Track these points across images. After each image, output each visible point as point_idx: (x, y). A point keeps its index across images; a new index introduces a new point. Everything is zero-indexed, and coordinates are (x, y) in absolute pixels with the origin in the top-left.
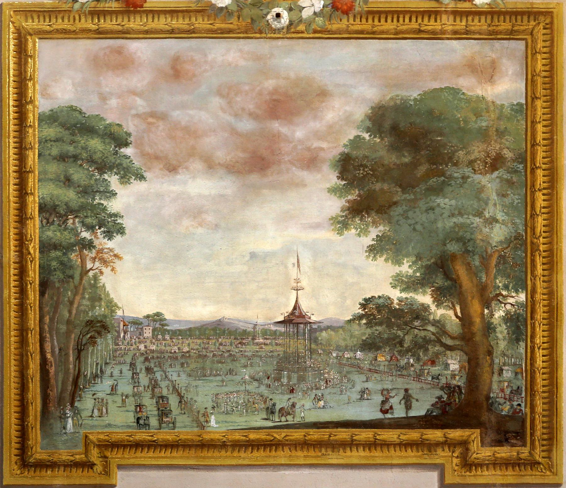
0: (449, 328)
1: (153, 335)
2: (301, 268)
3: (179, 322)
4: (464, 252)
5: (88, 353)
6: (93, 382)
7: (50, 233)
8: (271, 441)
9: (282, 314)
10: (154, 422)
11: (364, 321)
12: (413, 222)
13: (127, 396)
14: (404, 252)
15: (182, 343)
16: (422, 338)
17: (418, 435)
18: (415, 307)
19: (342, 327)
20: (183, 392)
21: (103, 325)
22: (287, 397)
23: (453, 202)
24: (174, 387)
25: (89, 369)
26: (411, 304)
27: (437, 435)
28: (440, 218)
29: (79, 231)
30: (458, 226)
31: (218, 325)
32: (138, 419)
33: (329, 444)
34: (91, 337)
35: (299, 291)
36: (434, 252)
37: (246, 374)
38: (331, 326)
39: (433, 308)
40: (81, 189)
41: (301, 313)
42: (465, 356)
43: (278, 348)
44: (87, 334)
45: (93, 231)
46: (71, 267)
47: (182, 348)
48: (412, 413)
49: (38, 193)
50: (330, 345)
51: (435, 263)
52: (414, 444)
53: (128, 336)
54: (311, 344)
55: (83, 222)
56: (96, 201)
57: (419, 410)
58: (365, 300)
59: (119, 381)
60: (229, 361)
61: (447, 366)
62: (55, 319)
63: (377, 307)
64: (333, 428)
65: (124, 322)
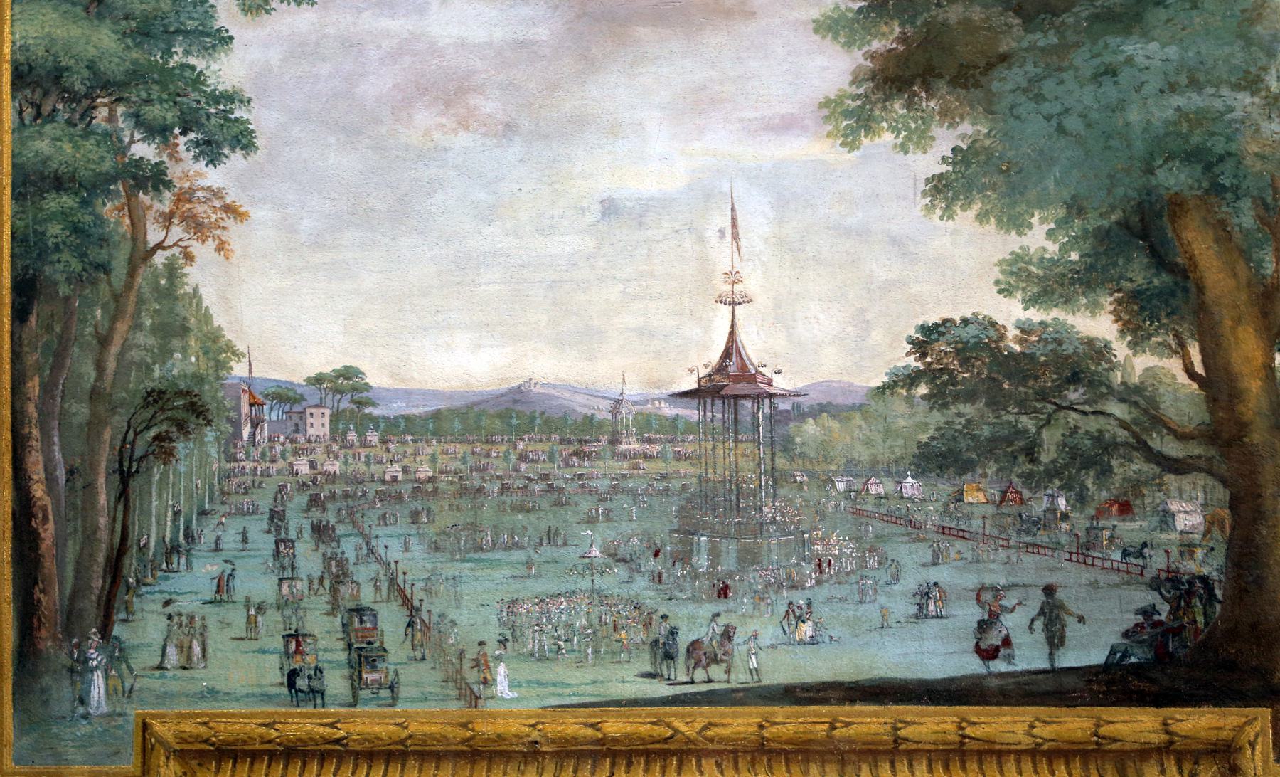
0: (1168, 408)
1: (334, 430)
2: (743, 242)
3: (408, 394)
4: (1207, 192)
5: (149, 483)
6: (164, 566)
7: (43, 146)
8: (666, 740)
9: (691, 371)
10: (336, 683)
11: (923, 390)
12: (1058, 108)
13: (260, 609)
14: (1031, 195)
15: (415, 454)
16: (1092, 438)
17: (1085, 725)
18: (1068, 349)
19: (859, 408)
20: (418, 595)
21: (193, 404)
22: (707, 609)
23: (1172, 52)
24: (392, 581)
25: (154, 529)
26: (1056, 337)
27: (1142, 726)
28: (1134, 96)
29: (127, 140)
30: (1188, 120)
31: (516, 401)
32: (293, 675)
33: (831, 752)
34: (158, 438)
35: (737, 308)
36: (1120, 191)
37: (594, 541)
38: (830, 404)
39: (1121, 350)
40: (133, 24)
41: (744, 367)
42: (1220, 488)
43: (684, 468)
44: (148, 428)
45: (165, 140)
46: (103, 241)
47: (413, 467)
48: (1069, 658)
49: (13, 33)
50: (827, 459)
51: (1124, 224)
52: (1075, 753)
53: (263, 435)
54: (773, 455)
55: (137, 116)
56: (176, 58)
57: (1087, 650)
58: (924, 329)
59: (237, 562)
60: (546, 506)
61: (1166, 519)
62: (56, 386)
63: (957, 351)
64: (841, 701)
65: (251, 395)
